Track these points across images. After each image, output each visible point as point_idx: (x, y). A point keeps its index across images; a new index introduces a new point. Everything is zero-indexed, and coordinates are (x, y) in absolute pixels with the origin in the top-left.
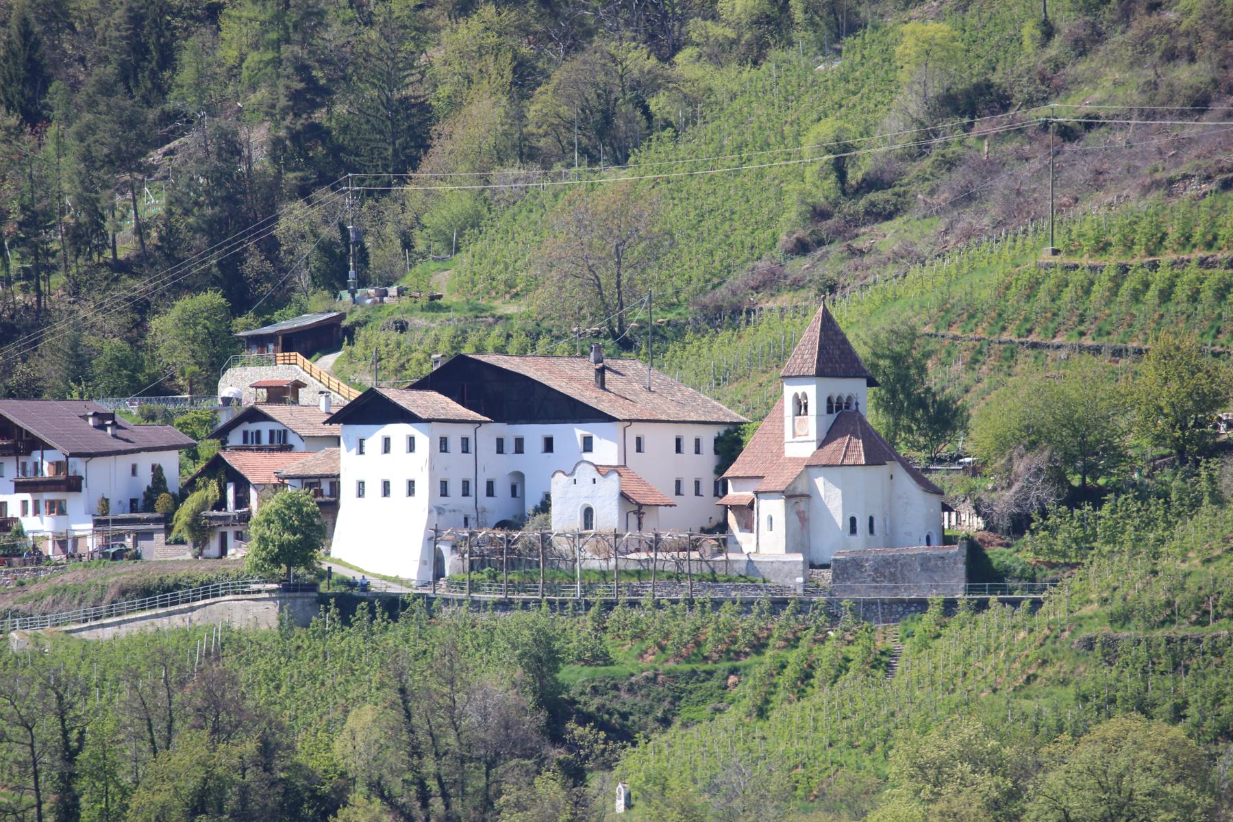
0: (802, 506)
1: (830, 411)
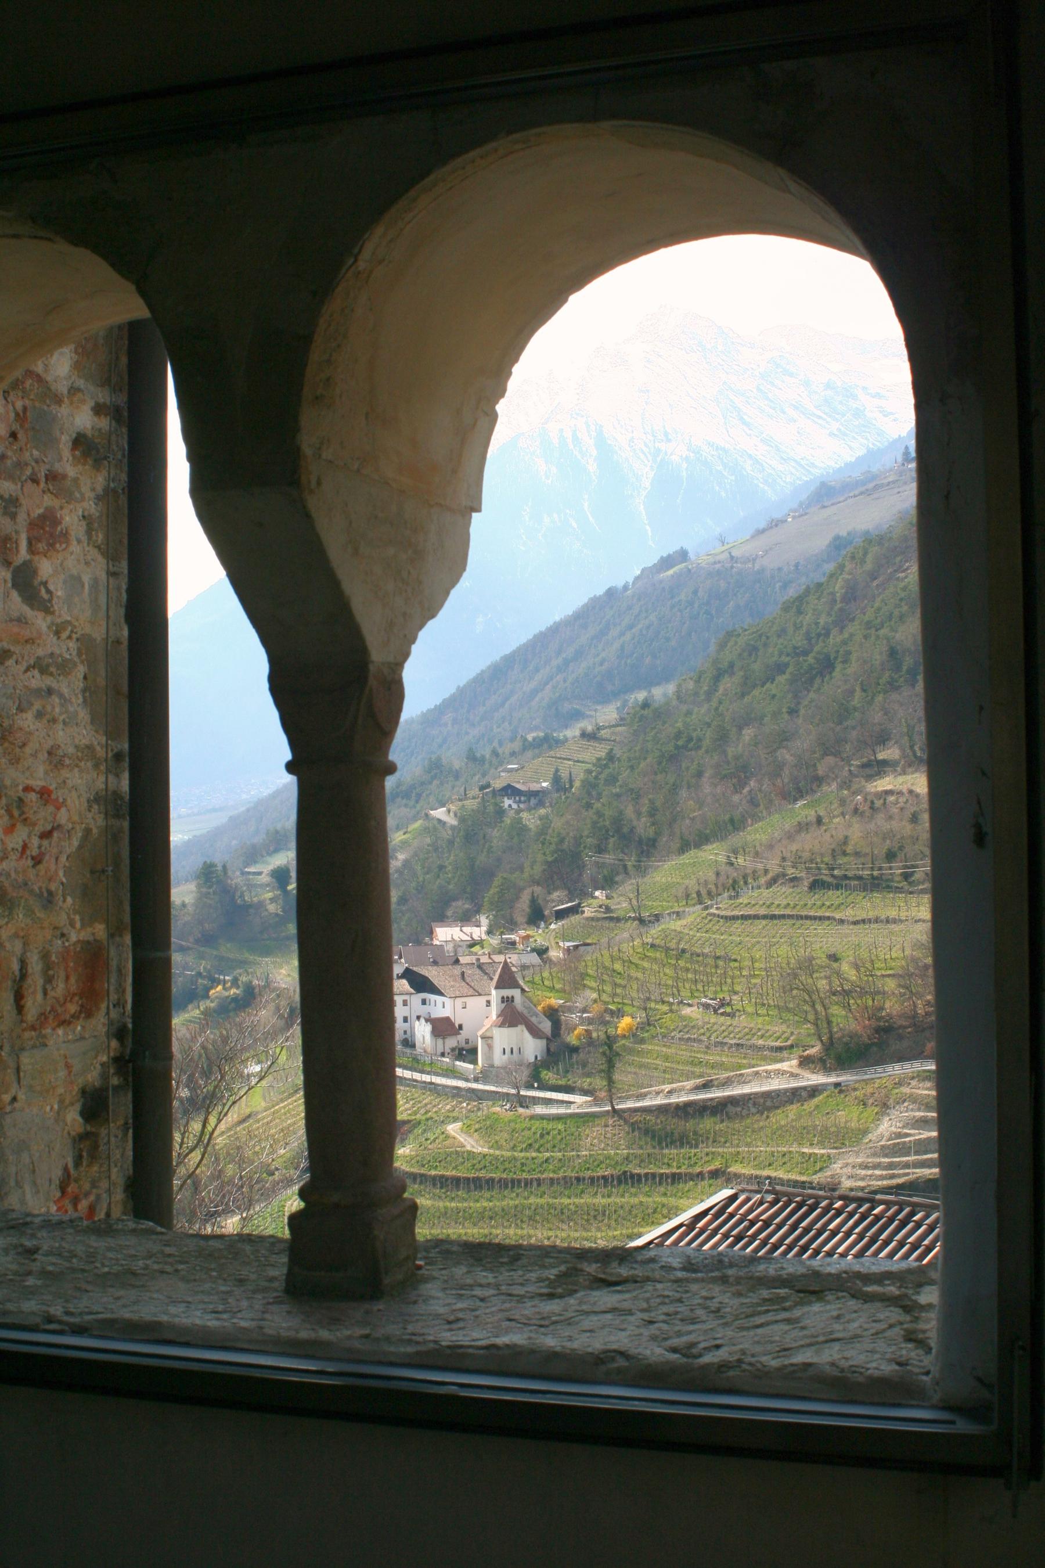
0: (490, 1041)
1: (503, 1002)
